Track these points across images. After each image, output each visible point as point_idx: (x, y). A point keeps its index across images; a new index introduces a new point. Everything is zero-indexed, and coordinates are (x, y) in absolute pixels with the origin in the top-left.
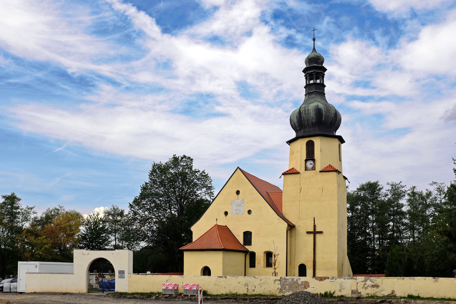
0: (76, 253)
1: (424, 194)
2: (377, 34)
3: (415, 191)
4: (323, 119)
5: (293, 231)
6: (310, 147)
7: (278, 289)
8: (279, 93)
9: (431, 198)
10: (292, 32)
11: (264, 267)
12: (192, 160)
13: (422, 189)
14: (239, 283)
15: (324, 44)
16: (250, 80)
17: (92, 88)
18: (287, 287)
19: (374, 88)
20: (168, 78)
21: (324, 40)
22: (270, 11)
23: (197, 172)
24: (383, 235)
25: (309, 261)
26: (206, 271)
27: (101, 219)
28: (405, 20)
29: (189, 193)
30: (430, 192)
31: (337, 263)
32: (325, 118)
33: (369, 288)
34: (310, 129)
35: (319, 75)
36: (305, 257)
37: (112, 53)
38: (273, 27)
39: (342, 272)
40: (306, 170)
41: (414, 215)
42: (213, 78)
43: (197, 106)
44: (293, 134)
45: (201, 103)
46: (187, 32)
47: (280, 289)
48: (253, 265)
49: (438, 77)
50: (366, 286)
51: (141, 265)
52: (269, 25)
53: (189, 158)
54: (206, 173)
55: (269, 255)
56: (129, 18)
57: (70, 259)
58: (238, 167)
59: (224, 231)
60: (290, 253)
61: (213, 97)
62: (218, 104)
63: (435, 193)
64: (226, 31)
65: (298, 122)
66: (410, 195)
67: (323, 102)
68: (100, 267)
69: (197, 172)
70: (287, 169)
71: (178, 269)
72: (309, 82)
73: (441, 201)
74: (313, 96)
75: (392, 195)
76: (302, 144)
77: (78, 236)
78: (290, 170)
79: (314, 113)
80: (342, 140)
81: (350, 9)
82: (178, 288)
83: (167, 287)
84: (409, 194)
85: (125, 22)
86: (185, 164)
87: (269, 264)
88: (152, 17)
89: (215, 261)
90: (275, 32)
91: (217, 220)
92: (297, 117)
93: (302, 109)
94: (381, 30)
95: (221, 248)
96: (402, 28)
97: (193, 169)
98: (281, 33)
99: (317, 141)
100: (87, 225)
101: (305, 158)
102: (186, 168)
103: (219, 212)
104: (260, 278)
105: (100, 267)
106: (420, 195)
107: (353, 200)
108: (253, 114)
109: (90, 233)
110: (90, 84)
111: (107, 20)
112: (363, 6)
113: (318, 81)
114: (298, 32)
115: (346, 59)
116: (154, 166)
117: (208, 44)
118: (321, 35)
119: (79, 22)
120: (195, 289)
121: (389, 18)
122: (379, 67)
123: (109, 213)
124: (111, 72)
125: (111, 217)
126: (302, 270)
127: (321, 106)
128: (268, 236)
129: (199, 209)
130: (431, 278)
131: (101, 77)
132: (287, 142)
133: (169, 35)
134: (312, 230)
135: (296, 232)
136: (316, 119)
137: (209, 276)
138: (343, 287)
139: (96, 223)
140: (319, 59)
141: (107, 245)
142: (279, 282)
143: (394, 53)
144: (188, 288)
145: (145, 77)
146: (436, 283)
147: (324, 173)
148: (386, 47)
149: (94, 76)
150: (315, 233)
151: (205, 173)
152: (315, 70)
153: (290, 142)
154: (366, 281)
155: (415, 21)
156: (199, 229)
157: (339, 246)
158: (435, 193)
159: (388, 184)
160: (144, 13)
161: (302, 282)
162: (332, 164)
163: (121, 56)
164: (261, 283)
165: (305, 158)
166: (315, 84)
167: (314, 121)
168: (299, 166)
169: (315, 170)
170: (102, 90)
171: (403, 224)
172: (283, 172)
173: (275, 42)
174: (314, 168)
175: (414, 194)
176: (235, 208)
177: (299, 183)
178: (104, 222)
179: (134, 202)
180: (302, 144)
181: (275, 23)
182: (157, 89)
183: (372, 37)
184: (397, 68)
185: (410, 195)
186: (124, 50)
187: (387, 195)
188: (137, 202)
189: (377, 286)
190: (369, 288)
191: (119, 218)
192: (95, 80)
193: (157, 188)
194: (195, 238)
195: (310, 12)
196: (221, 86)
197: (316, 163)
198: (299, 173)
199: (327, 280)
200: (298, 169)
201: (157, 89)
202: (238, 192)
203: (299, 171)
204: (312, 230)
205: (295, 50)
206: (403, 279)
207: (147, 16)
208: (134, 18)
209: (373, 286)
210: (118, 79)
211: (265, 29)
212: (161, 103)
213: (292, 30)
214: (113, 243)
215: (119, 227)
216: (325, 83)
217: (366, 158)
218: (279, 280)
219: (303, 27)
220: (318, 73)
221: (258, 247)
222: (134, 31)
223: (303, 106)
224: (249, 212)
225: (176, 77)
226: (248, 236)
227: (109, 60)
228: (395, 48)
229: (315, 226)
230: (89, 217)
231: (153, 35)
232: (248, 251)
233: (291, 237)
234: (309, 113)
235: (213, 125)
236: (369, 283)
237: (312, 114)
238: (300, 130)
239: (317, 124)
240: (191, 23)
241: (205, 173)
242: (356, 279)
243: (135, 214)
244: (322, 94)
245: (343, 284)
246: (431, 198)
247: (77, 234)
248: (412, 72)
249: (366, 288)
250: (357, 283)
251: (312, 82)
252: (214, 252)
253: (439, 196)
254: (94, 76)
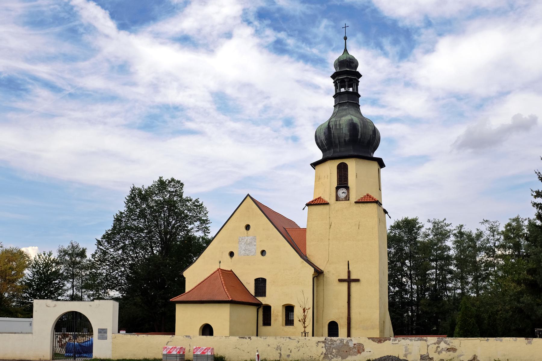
0: (38, 304)
1: (474, 235)
2: (386, 42)
3: (462, 231)
4: (359, 137)
5: (321, 277)
6: (343, 171)
7: (322, 354)
8: (266, 108)
9: (482, 239)
10: (282, 35)
11: (283, 326)
12: (182, 184)
13: (471, 228)
14: (269, 345)
15: (321, 51)
16: (229, 91)
17: (24, 93)
18: (334, 351)
19: (383, 106)
20: (125, 84)
21: (322, 46)
22: (252, 9)
23: (188, 201)
24: (428, 284)
25: (342, 318)
26: (207, 330)
27: (53, 260)
28: (419, 28)
29: (178, 227)
30: (481, 233)
31: (378, 320)
32: (361, 135)
33: (444, 352)
34: (343, 149)
35: (352, 82)
36: (336, 312)
37: (52, 50)
38: (258, 29)
39: (384, 333)
40: (337, 200)
41: (461, 262)
42: (183, 87)
43: (161, 120)
44: (319, 155)
45: (167, 117)
46: (150, 29)
47: (325, 354)
48: (267, 321)
49: (460, 97)
50: (439, 349)
51: (129, 323)
52: (252, 26)
53: (178, 182)
54: (200, 203)
55: (289, 309)
56: (75, 9)
57: (28, 312)
58: (248, 195)
59: (229, 277)
60: (317, 307)
61: (182, 110)
62: (189, 119)
63: (487, 233)
64: (199, 30)
65: (326, 139)
66: (456, 236)
67: (358, 115)
68: (72, 325)
69: (188, 201)
70: (311, 199)
71: (168, 327)
72: (340, 90)
73: (495, 243)
74: (345, 107)
75: (434, 236)
76: (332, 167)
77: (21, 282)
78: (315, 200)
79: (347, 128)
80: (381, 163)
81: (350, 11)
82: (184, 353)
83: (169, 352)
84: (455, 235)
85: (69, 14)
86: (172, 190)
87: (289, 322)
88: (105, 9)
89: (219, 316)
90: (259, 34)
91: (220, 263)
92: (325, 133)
93: (332, 124)
94: (390, 38)
95: (228, 299)
96: (415, 37)
97: (184, 196)
98: (267, 36)
99: (352, 165)
100: (34, 268)
101: (336, 185)
102: (174, 195)
103: (222, 253)
104: (297, 340)
105: (72, 325)
106: (469, 236)
107: (392, 240)
108: (233, 132)
109: (38, 279)
110: (22, 88)
111: (45, 9)
112: (367, 10)
113: (351, 90)
114: (290, 35)
115: (372, 68)
116: (133, 190)
117: (177, 46)
118: (318, 40)
119: (7, 9)
120: (210, 354)
121: (400, 25)
122: (388, 81)
123: (66, 253)
124: (51, 74)
125: (67, 258)
126: (333, 329)
127: (356, 120)
128: (288, 286)
129: (194, 248)
130: (523, 339)
131: (36, 79)
132: (311, 165)
133: (127, 32)
134: (346, 278)
135: (325, 279)
136: (350, 136)
137: (209, 337)
138: (410, 351)
139: (47, 265)
140: (353, 63)
141: (60, 295)
142: (323, 345)
143: (406, 66)
144: (199, 353)
145: (95, 83)
146: (529, 345)
147: (360, 205)
148: (397, 58)
149: (27, 78)
150: (349, 281)
151: (198, 202)
152: (347, 76)
153: (314, 165)
154: (438, 343)
155: (431, 31)
156: (194, 275)
157: (380, 298)
158: (487, 233)
159: (429, 221)
160: (95, 3)
161: (355, 344)
162: (370, 194)
163: (64, 55)
164: (298, 345)
165: (336, 185)
166: (347, 92)
167: (347, 139)
168: (329, 195)
169: (349, 200)
170: (38, 96)
171: (451, 272)
172: (308, 202)
173: (260, 46)
175: (461, 234)
176: (243, 248)
177: (328, 217)
178: (58, 263)
179: (104, 237)
180: (332, 167)
181: (260, 24)
182: (110, 98)
183: (379, 46)
184: (410, 84)
185: (456, 236)
186: (67, 47)
187: (429, 235)
188: (108, 237)
189: (454, 350)
190: (444, 352)
191: (78, 259)
192: (29, 83)
193: (135, 220)
194: (188, 287)
195: (304, 14)
196: (192, 96)
197: (350, 191)
198: (328, 204)
199: (388, 341)
200: (327, 199)
201: (110, 98)
202: (248, 227)
203: (328, 202)
204: (346, 278)
205: (286, 58)
206: (487, 340)
207: (99, 8)
208: (82, 9)
209: (448, 350)
210: (59, 83)
211: (248, 31)
212: (114, 115)
213: (282, 33)
214: (70, 292)
215: (78, 270)
216: (359, 93)
217: (432, 184)
218: (323, 342)
219: (295, 30)
220: (351, 80)
221: (274, 299)
222: (81, 25)
223: (333, 119)
224: (263, 253)
225: (134, 84)
226: (261, 284)
227: (48, 59)
228: (408, 61)
229: (349, 272)
230: (38, 257)
231: (107, 31)
232: (262, 304)
233: (317, 286)
234: (341, 129)
235: (182, 145)
236: (443, 345)
237: (345, 130)
238: (329, 149)
239: (349, 143)
240: (154, 19)
241: (198, 202)
242: (426, 340)
243: (105, 253)
244: (357, 106)
245: (409, 347)
246: (482, 239)
247: (20, 280)
248: (428, 89)
249: (439, 353)
250: (428, 346)
251: (343, 90)
252: (238, 305)
253: (492, 238)
254: (27, 78)
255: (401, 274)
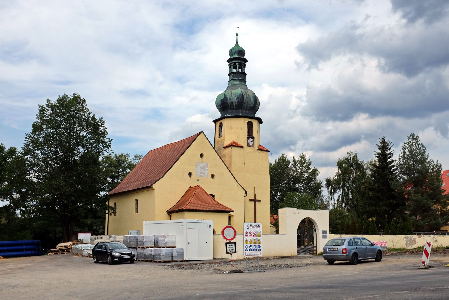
34: (247, 112)
58: (202, 131)
103: (184, 172)
134: (253, 198)
147: (260, 151)
174: (253, 146)
202: (201, 155)
204: (253, 198)
224: (213, 176)
229: (255, 195)
237: (235, 100)
255: (26, 193)
